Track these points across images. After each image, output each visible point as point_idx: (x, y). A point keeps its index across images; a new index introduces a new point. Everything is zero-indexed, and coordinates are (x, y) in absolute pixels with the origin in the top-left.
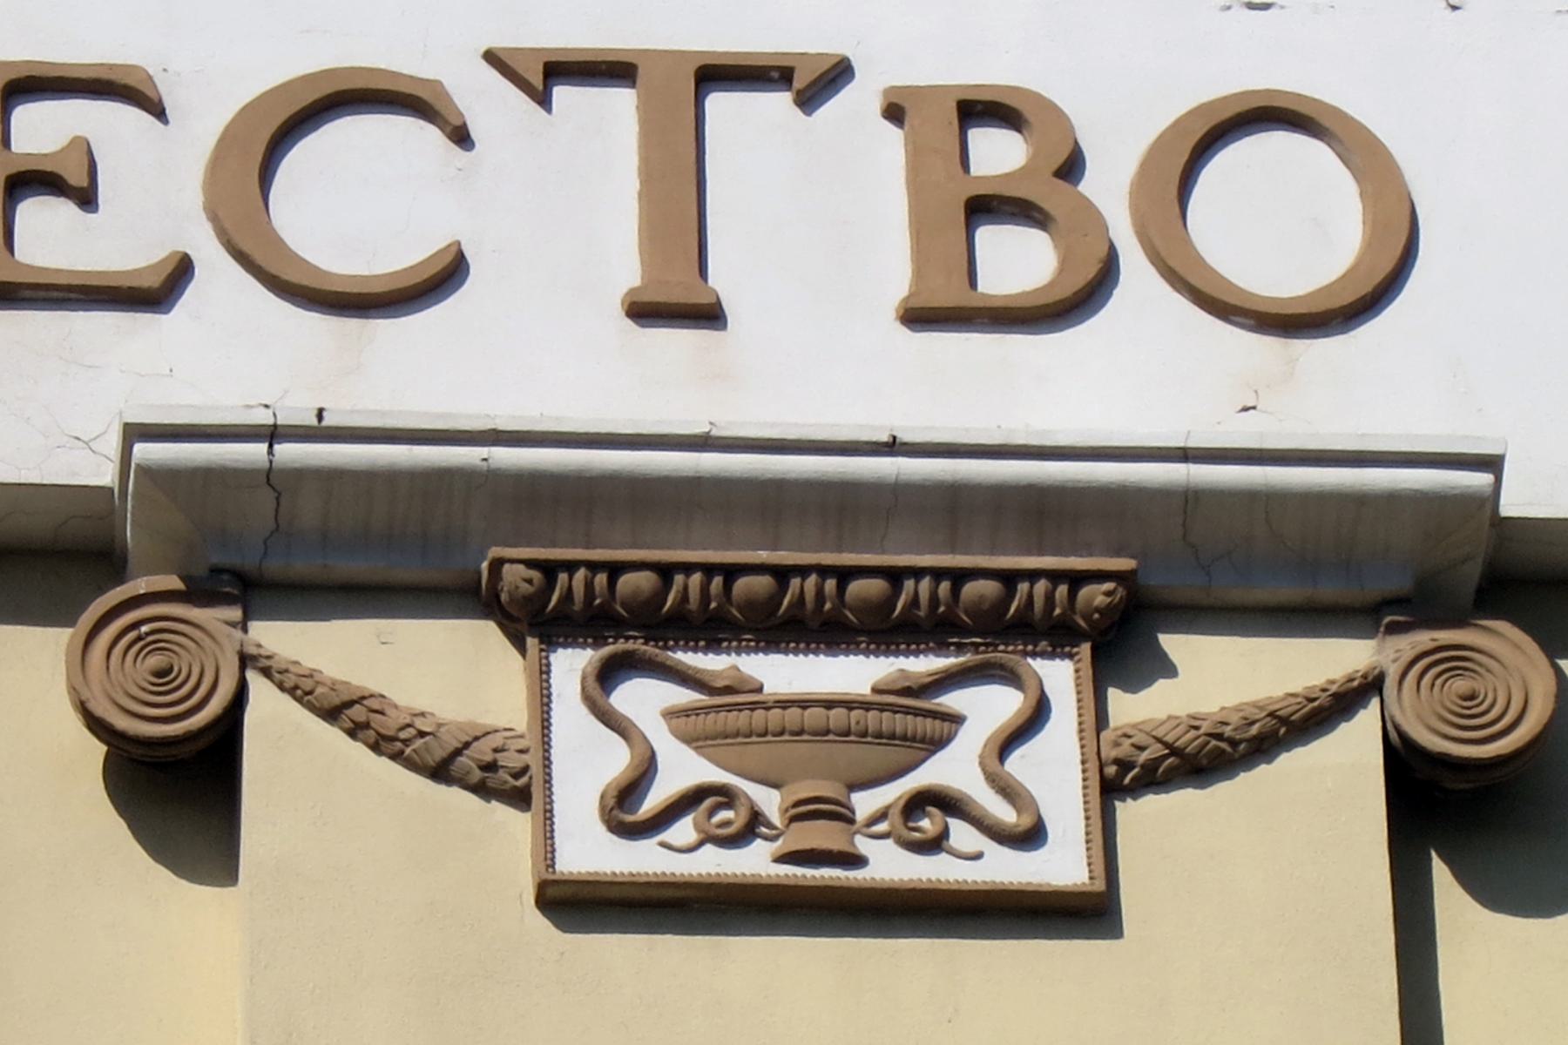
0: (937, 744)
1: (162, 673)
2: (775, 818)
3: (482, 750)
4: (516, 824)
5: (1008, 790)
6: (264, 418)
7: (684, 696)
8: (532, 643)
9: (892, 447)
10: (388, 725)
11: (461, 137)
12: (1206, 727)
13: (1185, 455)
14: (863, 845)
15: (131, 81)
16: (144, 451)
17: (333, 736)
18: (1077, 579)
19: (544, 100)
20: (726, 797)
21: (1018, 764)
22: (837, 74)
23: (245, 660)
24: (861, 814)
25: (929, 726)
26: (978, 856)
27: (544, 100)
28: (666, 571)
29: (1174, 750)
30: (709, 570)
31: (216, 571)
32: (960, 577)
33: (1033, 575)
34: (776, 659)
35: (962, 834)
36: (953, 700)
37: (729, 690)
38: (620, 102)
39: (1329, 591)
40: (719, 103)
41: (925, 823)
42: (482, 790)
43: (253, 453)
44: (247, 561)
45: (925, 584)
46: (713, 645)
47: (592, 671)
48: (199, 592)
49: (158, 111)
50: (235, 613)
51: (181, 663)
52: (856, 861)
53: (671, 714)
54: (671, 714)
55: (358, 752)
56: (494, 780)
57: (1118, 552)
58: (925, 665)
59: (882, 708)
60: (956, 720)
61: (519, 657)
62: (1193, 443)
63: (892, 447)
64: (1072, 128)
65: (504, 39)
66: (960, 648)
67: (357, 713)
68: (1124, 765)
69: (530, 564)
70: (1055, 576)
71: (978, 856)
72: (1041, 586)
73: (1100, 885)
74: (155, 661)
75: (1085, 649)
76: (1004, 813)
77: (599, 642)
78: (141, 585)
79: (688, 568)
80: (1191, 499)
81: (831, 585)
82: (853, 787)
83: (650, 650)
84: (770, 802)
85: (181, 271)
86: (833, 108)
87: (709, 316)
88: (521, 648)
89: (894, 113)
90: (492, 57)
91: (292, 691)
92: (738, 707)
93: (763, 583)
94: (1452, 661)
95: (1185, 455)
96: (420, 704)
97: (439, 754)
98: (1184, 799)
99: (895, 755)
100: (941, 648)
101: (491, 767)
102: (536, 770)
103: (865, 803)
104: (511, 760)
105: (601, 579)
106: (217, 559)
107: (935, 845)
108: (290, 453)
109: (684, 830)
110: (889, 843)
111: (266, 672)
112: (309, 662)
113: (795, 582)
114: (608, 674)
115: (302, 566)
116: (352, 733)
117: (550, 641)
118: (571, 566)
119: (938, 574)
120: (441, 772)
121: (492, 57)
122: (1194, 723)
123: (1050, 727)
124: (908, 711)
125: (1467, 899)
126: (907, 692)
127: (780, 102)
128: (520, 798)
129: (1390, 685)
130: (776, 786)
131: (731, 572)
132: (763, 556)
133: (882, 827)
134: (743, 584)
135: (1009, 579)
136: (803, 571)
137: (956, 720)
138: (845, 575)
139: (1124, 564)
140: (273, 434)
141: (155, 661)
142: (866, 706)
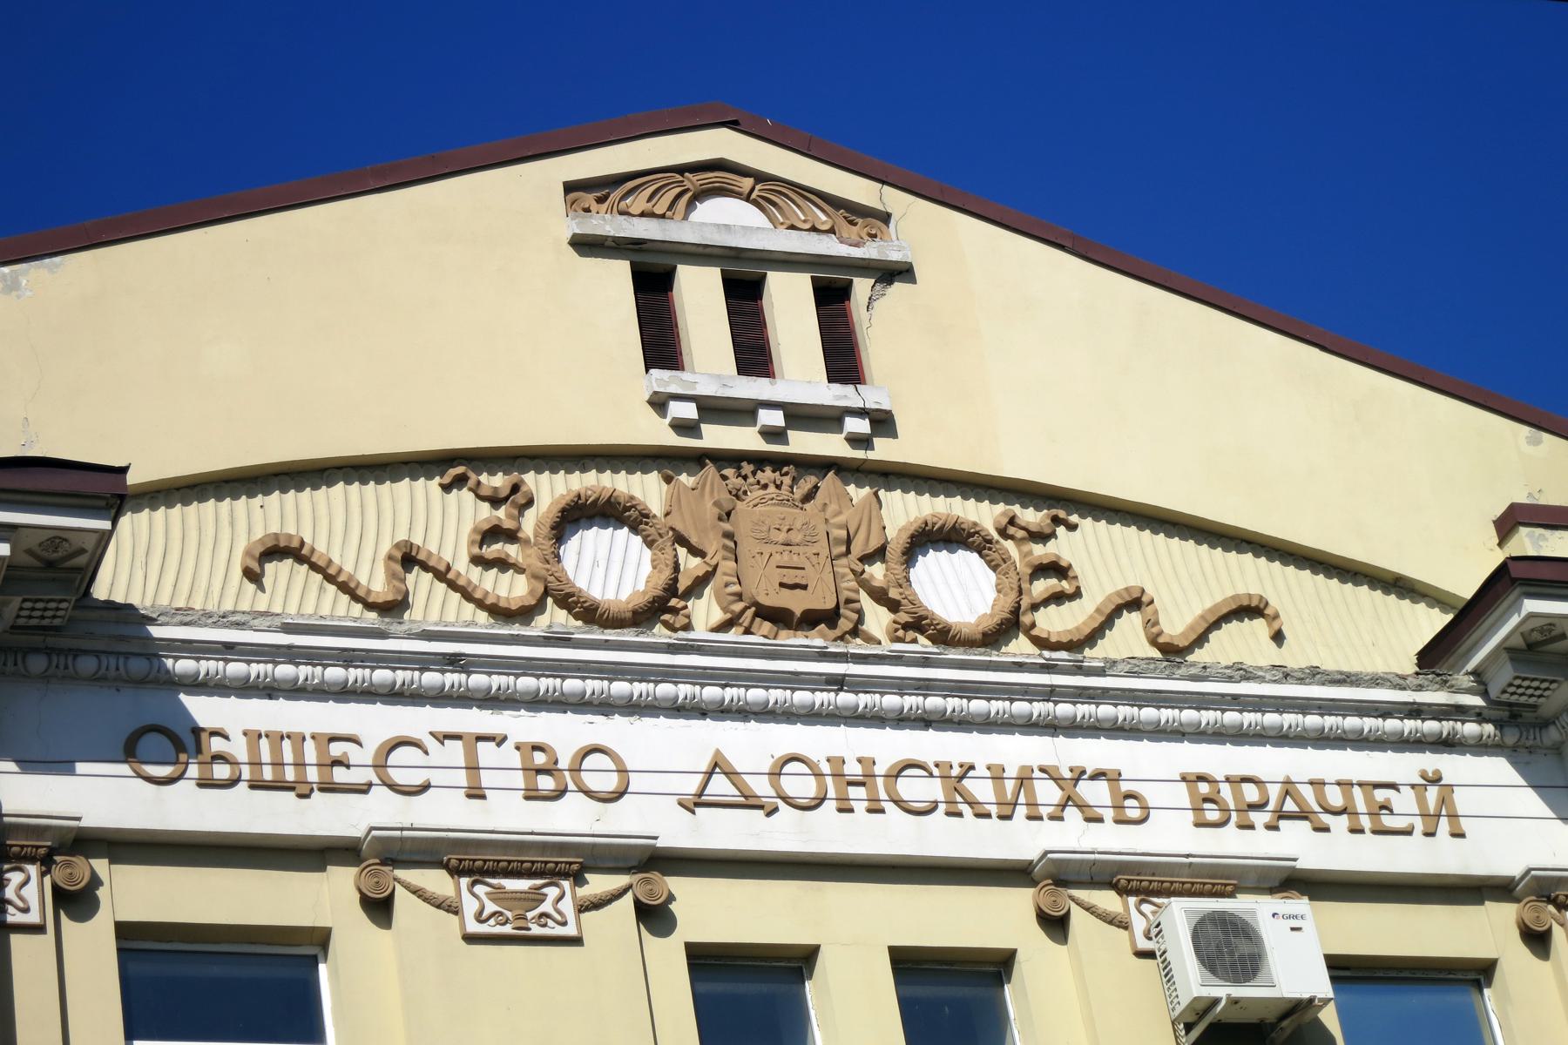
0: (543, 901)
1: (1538, 917)
2: (511, 919)
3: (448, 902)
4: (454, 919)
5: (21, 898)
6: (401, 826)
7: (488, 889)
8: (456, 876)
9: (532, 833)
10: (427, 895)
11: (426, 753)
12: (598, 898)
13: (593, 836)
14: (530, 925)
15: (418, 742)
16: (374, 833)
17: (414, 897)
18: (571, 863)
19: (443, 744)
20: (501, 914)
21: (560, 906)
22: (505, 738)
23: (395, 879)
24: (529, 918)
25: (541, 897)
26: (14, 915)
27: (443, 744)
28: (485, 861)
29: (592, 903)
30: (494, 861)
31: (387, 859)
32: (546, 863)
33: (562, 862)
34: (507, 880)
35: (550, 923)
36: (545, 890)
37: (499, 888)
38: (459, 743)
39: (621, 865)
40: (480, 744)
41: (542, 920)
42: (448, 911)
43: (398, 833)
44: (393, 857)
45: (539, 864)
46: (494, 877)
47: (470, 884)
48: (383, 863)
49: (361, 745)
50: (391, 868)
51: (1059, 900)
52: (529, 929)
53: (487, 894)
54: (487, 894)
55: (420, 901)
56: (450, 909)
57: (578, 857)
58: (539, 882)
59: (529, 893)
60: (546, 895)
61: (450, 878)
62: (595, 833)
63: (532, 833)
64: (556, 754)
65: (433, 730)
66: (545, 878)
67: (420, 893)
68: (582, 906)
69: (457, 859)
70: (566, 863)
71: (14, 915)
72: (563, 865)
73: (42, 923)
74: (376, 880)
75: (39, 863)
76: (21, 904)
77: (470, 876)
78: (371, 861)
79: (489, 860)
80: (594, 845)
81: (519, 864)
82: (527, 911)
83: (480, 878)
84: (509, 914)
85: (370, 785)
86: (504, 746)
87: (1462, 836)
88: (453, 877)
89: (518, 748)
90: (431, 733)
91: (405, 887)
92: (502, 893)
93: (1210, 886)
94: (647, 881)
95: (593, 836)
96: (433, 891)
97: (439, 903)
98: (593, 913)
99: (534, 904)
100: (541, 878)
101: (450, 906)
102: (460, 907)
103: (530, 915)
104: (455, 905)
105: (471, 863)
106: (388, 856)
107: (545, 925)
108: (406, 833)
109: (492, 921)
110: (535, 925)
111: (399, 882)
112: (409, 880)
113: (559, 865)
114: (1143, 901)
115: (405, 857)
116: (1092, 914)
117: (460, 876)
118: (465, 860)
119: (542, 862)
120: (439, 907)
121: (431, 733)
122: (596, 896)
123: (30, 883)
124: (535, 893)
125: (648, 934)
126: (535, 889)
127: (492, 744)
128: (456, 913)
129: (634, 886)
130: (510, 911)
131: (499, 861)
132: (505, 858)
133: (533, 921)
134: (501, 864)
135: (557, 863)
136: (514, 861)
137: (546, 895)
138: (522, 862)
139: (581, 860)
140: (402, 829)
141: (376, 880)
142: (525, 893)
